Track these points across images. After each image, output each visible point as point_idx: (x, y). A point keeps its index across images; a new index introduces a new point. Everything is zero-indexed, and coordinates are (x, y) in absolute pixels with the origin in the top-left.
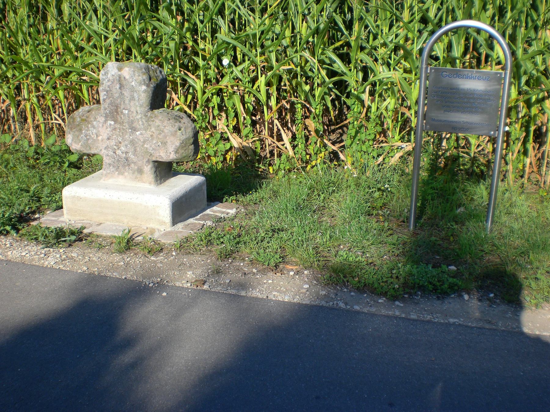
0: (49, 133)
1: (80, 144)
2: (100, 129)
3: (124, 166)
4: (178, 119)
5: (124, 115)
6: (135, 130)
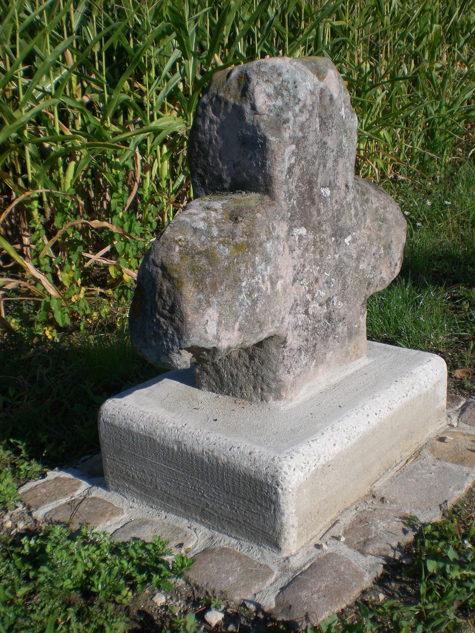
6: (341, 236)
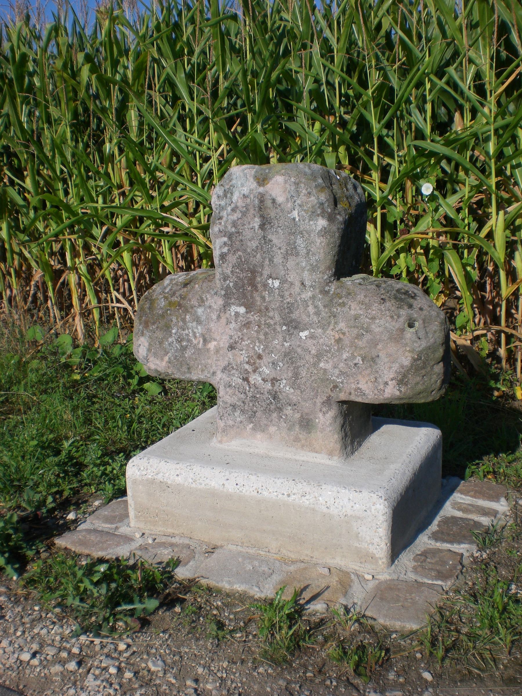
0: (108, 322)
1: (166, 358)
2: (212, 325)
3: (267, 411)
4: (403, 299)
5: (271, 291)
6: (296, 328)
